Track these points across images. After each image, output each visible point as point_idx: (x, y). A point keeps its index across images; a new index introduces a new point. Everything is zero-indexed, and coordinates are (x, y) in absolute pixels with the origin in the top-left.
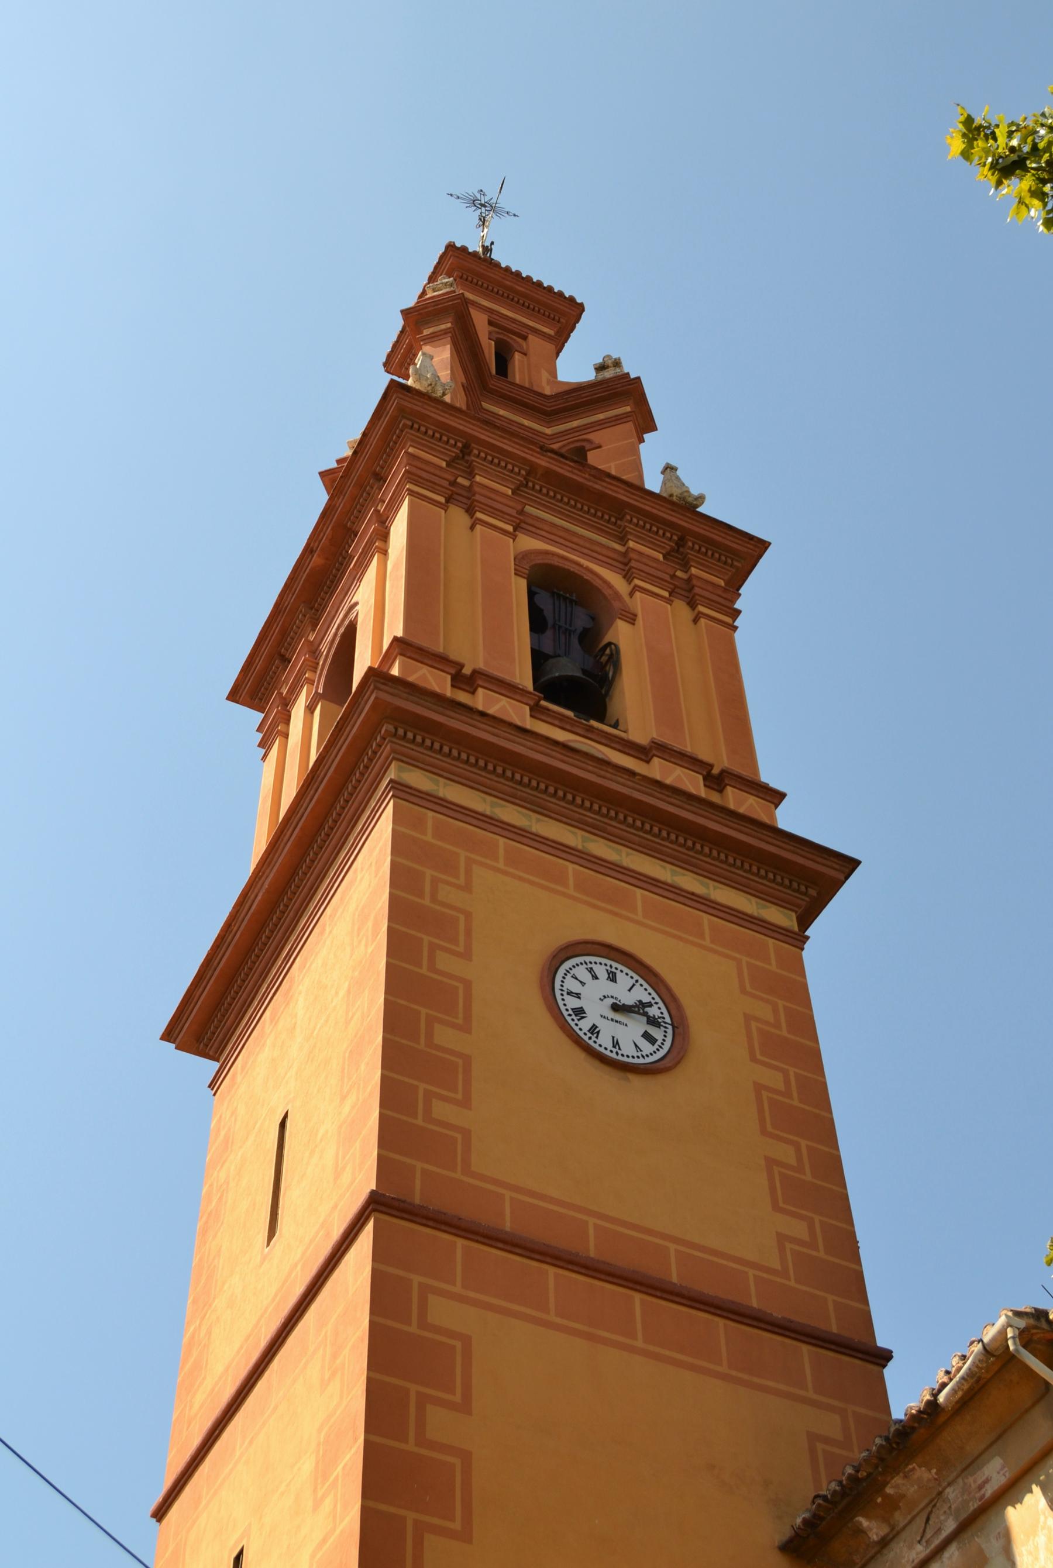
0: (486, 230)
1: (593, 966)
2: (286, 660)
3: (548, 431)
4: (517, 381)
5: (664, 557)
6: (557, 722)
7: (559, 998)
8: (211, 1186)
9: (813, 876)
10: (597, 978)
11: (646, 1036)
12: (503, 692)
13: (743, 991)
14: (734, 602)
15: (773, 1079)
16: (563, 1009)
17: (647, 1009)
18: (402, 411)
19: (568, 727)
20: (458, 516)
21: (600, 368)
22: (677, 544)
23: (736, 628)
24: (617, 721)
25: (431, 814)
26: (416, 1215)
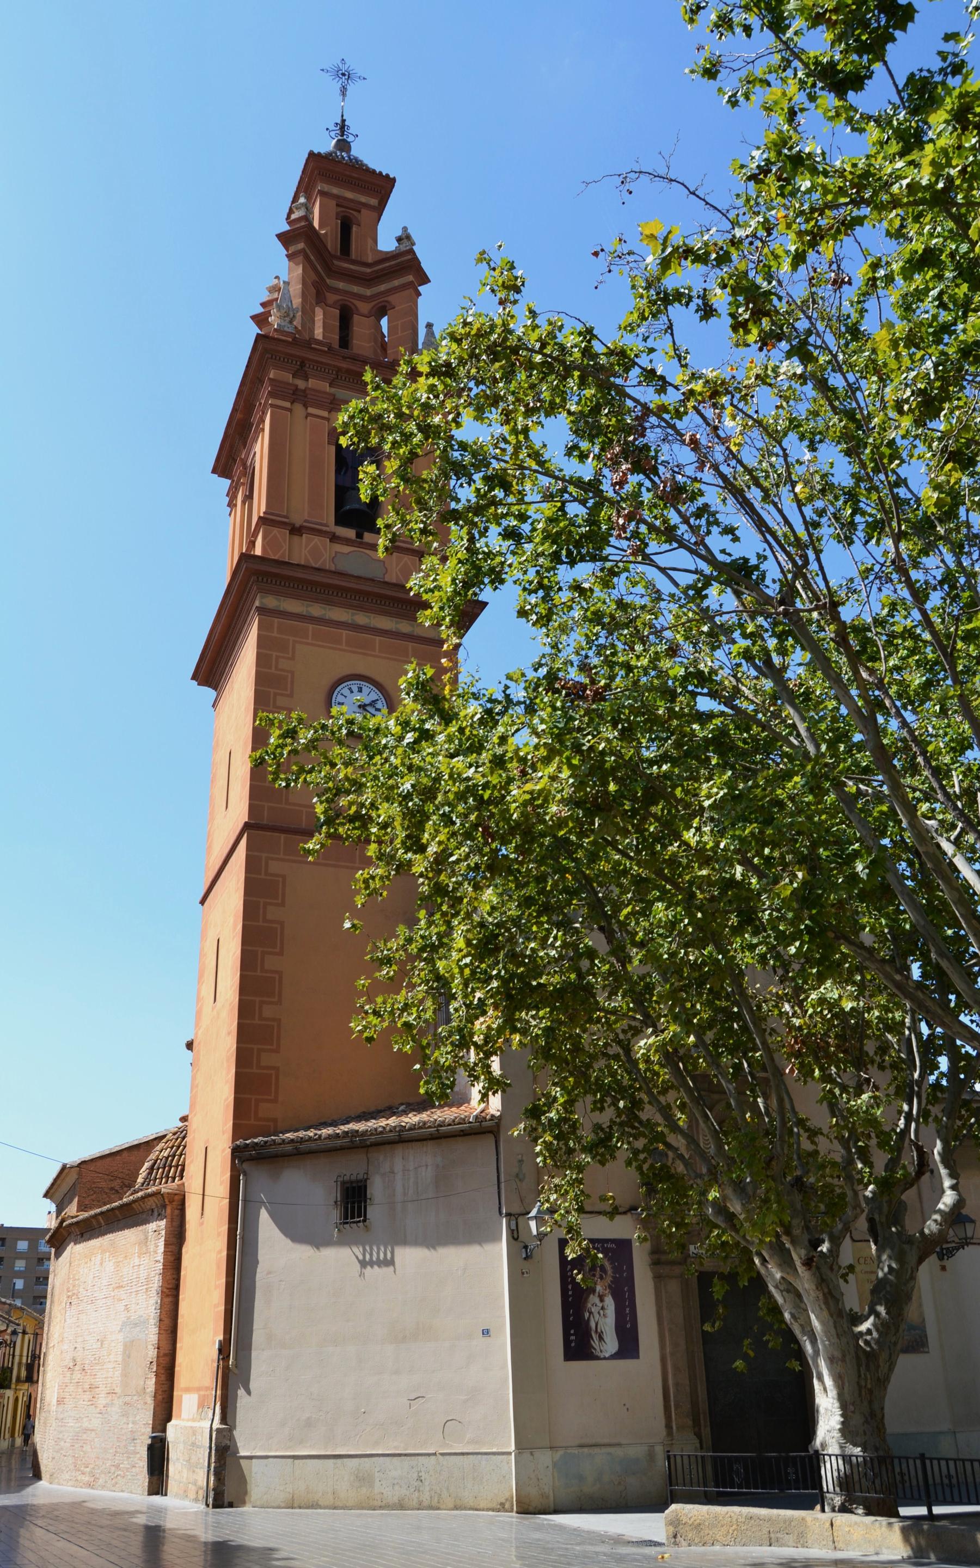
3: (368, 292)
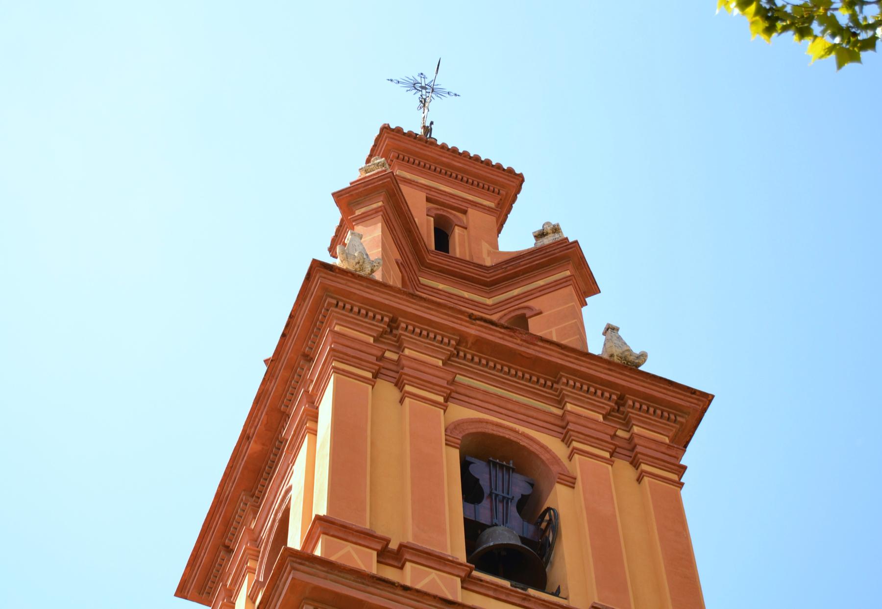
0: (426, 111)
2: (229, 550)
4: (458, 255)
5: (605, 418)
6: (491, 593)
14: (679, 458)
18: (326, 290)
19: (503, 597)
20: (387, 390)
21: (540, 235)
22: (616, 403)
23: (683, 484)
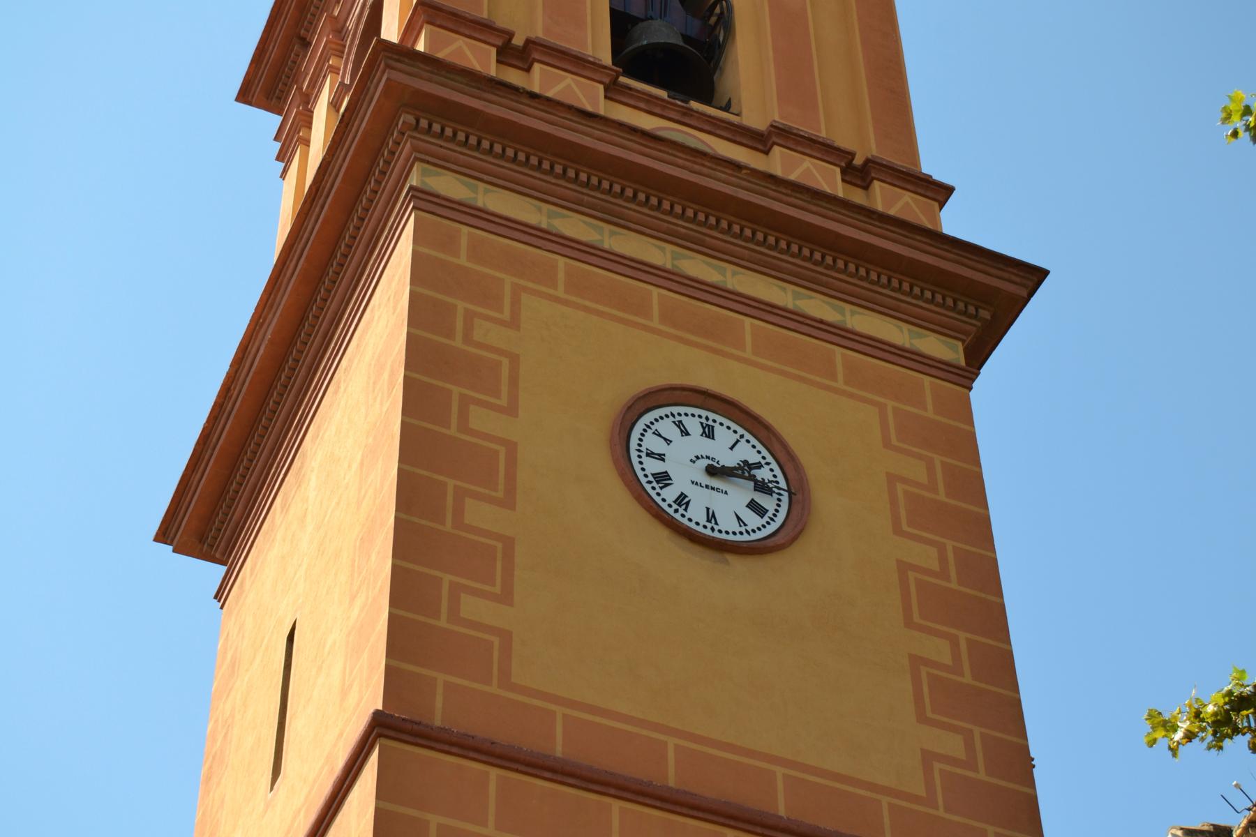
1: (683, 418)
2: (306, 44)
6: (642, 105)
7: (635, 460)
8: (216, 721)
9: (987, 295)
10: (688, 434)
11: (754, 506)
12: (569, 68)
13: (887, 444)
15: (925, 556)
16: (640, 474)
17: (753, 472)
19: (657, 110)
24: (730, 101)
25: (465, 229)
26: (437, 740)
